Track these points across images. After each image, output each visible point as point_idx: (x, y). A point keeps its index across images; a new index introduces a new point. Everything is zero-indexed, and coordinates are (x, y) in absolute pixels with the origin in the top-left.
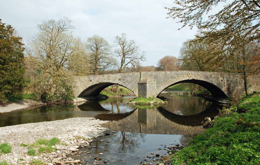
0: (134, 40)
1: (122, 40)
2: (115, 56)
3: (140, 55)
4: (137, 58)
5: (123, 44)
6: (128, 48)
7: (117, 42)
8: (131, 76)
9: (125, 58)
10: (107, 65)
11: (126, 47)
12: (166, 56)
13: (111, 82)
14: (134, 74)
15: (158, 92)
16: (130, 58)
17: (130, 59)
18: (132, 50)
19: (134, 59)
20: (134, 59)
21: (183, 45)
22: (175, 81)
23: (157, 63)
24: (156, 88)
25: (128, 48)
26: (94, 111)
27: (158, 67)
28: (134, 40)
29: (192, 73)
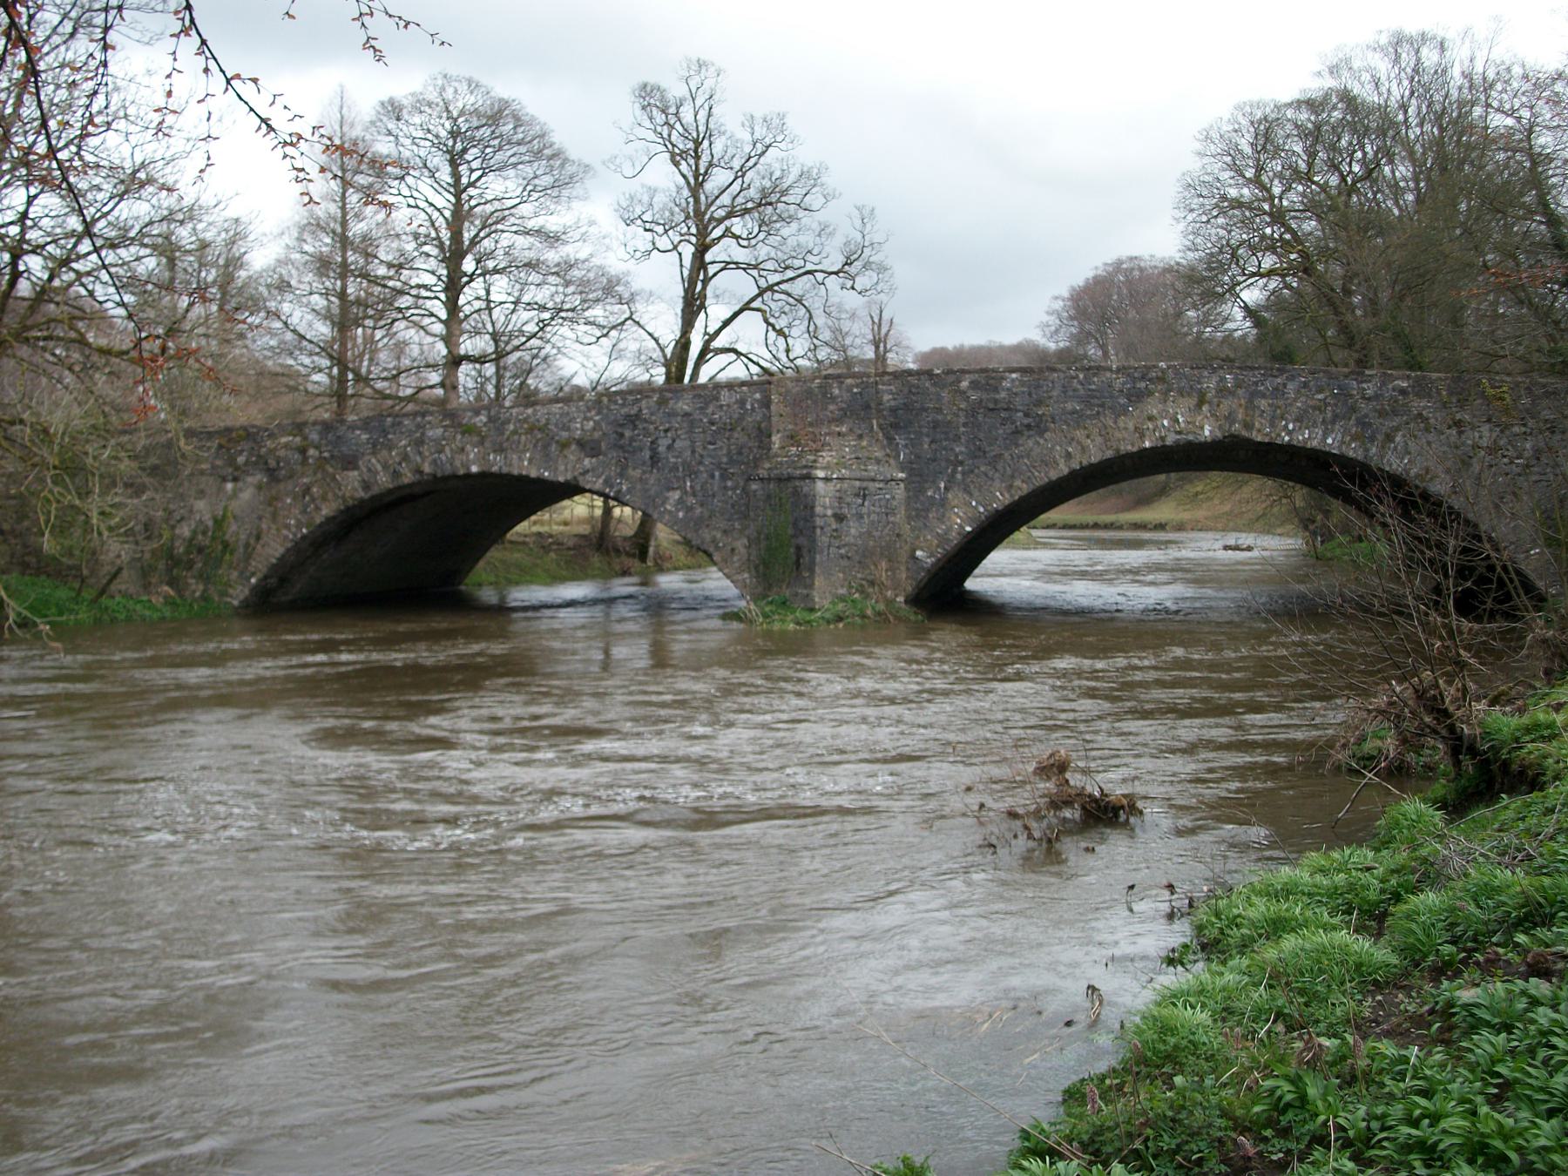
0: (782, 116)
1: (687, 114)
2: (622, 253)
3: (838, 240)
4: (809, 267)
5: (691, 154)
6: (736, 187)
7: (651, 136)
8: (687, 414)
9: (712, 270)
10: (543, 325)
11: (719, 178)
12: (1119, 263)
13: (516, 472)
14: (717, 399)
15: (919, 553)
16: (755, 267)
17: (754, 273)
18: (767, 205)
19: (790, 274)
20: (790, 274)
21: (1201, 155)
22: (1069, 456)
23: (1046, 318)
24: (909, 518)
25: (736, 187)
26: (999, 600)
27: (1052, 346)
28: (782, 116)
29: (1223, 379)
